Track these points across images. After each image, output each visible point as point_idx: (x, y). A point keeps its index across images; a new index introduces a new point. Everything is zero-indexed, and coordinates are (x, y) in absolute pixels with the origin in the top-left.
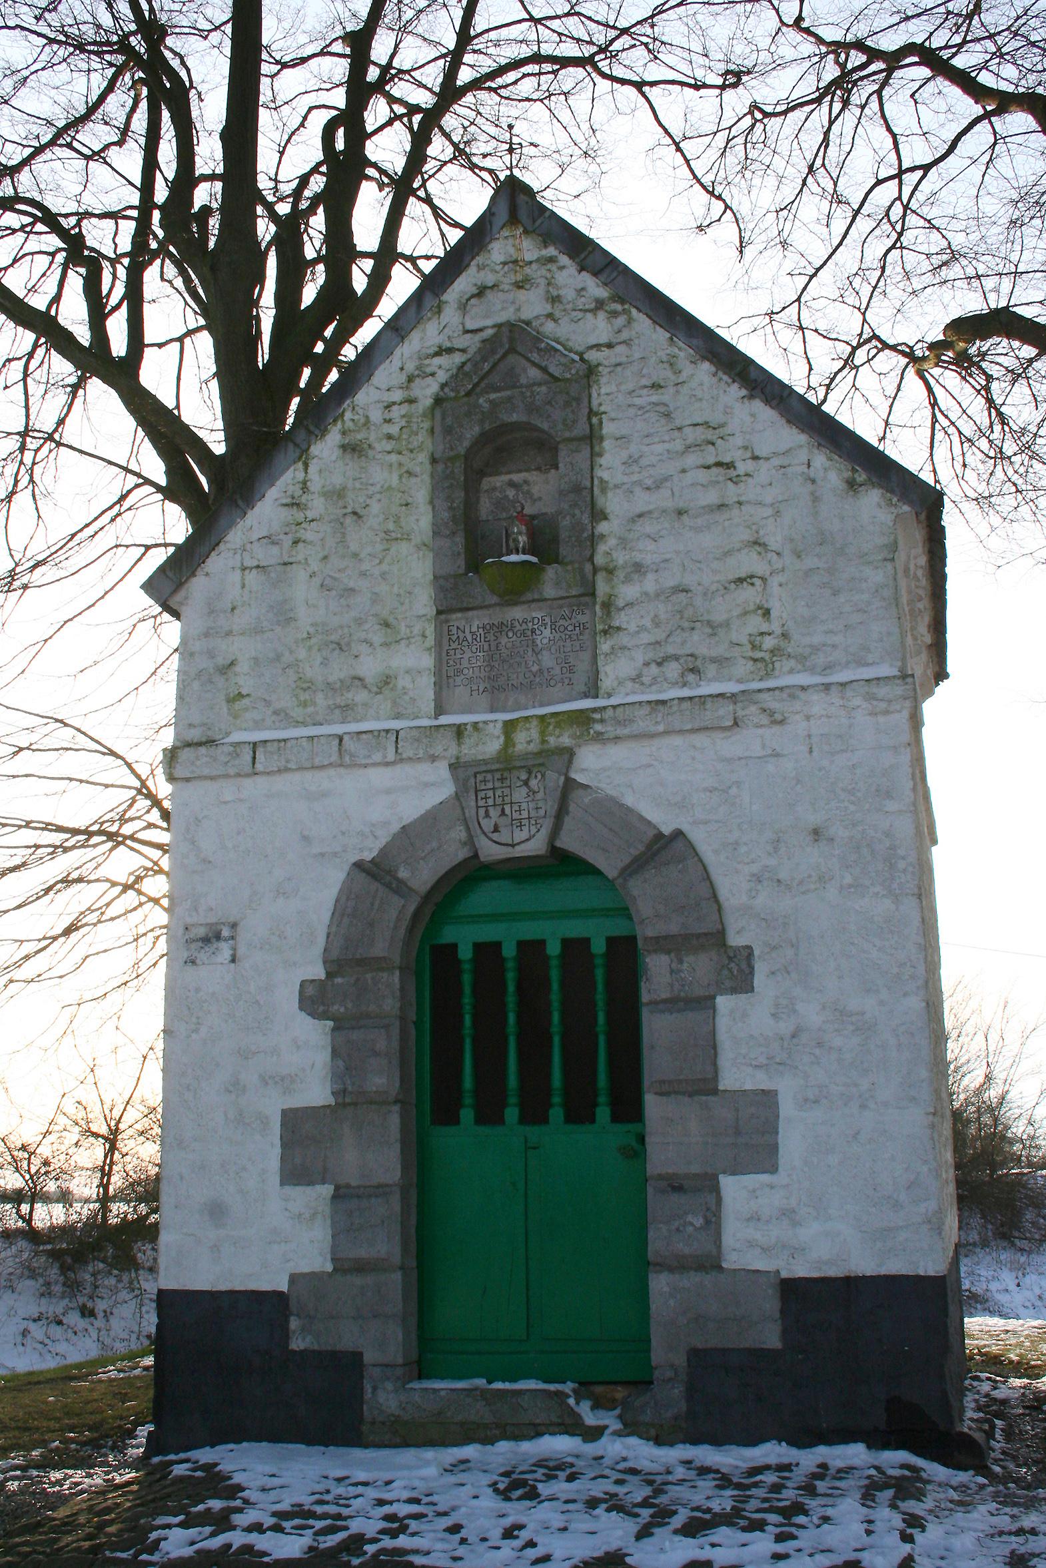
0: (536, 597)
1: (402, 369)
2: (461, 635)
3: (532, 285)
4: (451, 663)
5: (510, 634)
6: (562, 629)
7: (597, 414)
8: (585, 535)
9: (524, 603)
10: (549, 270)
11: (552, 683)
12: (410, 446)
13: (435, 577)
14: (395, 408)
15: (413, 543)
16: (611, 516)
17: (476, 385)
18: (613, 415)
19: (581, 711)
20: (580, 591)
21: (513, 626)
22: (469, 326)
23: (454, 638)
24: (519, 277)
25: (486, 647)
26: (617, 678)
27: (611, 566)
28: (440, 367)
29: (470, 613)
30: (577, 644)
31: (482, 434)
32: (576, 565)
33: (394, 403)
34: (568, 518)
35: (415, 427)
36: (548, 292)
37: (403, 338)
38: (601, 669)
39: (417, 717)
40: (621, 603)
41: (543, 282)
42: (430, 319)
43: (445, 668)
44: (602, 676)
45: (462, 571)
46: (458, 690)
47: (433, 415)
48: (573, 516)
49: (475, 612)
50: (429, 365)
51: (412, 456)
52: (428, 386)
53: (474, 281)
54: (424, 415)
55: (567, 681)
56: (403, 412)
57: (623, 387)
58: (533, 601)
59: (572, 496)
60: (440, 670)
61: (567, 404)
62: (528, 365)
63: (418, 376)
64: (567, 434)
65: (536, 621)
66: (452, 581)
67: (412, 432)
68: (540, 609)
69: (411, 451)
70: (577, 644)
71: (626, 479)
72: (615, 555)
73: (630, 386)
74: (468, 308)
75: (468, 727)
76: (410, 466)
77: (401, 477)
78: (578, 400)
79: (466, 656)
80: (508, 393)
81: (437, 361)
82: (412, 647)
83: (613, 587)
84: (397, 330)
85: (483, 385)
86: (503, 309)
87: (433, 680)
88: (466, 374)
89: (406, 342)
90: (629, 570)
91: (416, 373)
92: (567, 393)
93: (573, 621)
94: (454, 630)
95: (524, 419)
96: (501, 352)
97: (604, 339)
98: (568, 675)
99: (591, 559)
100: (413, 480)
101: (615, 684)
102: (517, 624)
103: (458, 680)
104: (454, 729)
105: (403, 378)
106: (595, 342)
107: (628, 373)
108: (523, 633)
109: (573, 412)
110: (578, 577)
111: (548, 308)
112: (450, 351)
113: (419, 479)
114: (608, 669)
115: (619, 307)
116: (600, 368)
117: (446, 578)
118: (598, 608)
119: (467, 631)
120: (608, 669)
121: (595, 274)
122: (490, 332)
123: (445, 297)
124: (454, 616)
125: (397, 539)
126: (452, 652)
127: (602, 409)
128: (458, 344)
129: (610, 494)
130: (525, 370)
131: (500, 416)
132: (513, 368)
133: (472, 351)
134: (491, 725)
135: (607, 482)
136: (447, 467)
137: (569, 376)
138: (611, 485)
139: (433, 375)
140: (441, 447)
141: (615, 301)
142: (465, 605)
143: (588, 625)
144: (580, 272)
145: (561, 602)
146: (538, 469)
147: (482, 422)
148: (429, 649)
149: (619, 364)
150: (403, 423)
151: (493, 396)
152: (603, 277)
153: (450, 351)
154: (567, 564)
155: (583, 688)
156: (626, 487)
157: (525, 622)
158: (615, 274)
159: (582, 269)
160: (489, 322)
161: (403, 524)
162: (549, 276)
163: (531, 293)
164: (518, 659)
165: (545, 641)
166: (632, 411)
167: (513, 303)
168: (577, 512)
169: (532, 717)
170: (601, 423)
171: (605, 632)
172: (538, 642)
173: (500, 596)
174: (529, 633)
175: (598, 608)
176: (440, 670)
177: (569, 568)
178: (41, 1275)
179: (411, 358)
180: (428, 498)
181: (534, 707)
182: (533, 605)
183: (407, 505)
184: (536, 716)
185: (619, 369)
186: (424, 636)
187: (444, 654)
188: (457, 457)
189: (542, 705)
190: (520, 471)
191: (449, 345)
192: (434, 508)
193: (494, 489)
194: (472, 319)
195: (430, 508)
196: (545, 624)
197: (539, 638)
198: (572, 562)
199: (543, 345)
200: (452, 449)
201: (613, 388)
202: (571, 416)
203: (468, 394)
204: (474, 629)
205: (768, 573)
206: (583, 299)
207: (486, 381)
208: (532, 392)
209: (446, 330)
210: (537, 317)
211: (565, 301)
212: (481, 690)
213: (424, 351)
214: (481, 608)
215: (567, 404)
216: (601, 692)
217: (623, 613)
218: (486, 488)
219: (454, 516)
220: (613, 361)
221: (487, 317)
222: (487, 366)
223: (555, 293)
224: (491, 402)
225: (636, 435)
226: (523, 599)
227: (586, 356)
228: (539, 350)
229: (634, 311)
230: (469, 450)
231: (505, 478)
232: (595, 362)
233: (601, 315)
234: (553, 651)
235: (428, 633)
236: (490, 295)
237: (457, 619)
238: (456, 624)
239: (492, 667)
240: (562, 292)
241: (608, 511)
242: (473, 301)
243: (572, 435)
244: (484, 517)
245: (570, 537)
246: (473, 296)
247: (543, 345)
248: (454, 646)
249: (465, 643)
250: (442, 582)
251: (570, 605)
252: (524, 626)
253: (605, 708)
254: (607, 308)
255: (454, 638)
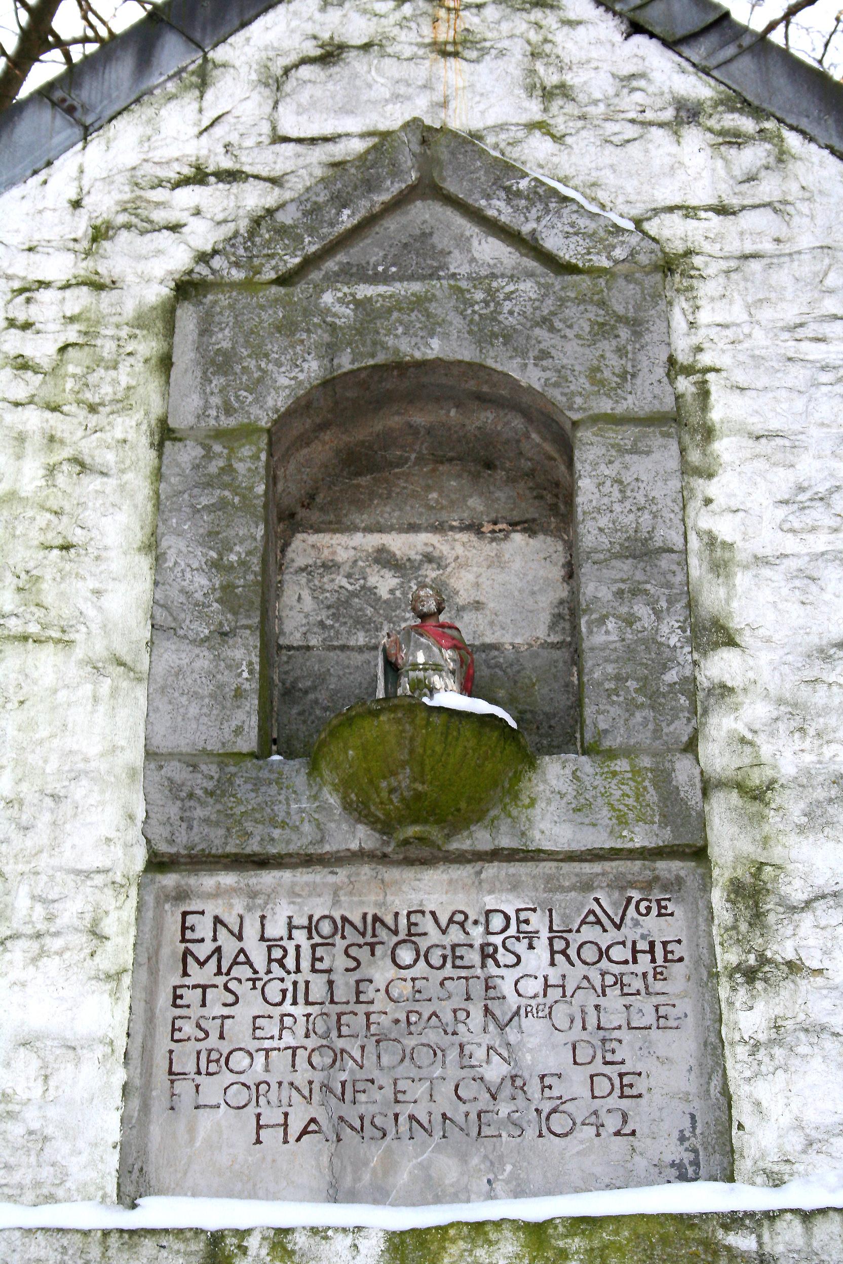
0: (506, 842)
1: (77, 204)
2: (230, 947)
3: (484, 52)
4: (188, 1029)
5: (406, 955)
6: (590, 954)
7: (688, 370)
8: (671, 676)
9: (461, 858)
10: (538, 26)
11: (559, 1123)
12: (88, 396)
13: (150, 755)
14: (44, 295)
15: (79, 652)
16: (745, 639)
17: (310, 262)
18: (740, 377)
19: (683, 1220)
20: (664, 837)
21: (413, 934)
22: (290, 125)
23: (202, 951)
24: (444, 34)
25: (318, 990)
26: (799, 1125)
27: (756, 778)
28: (197, 213)
29: (267, 878)
30: (646, 1005)
31: (328, 384)
32: (646, 762)
33: (43, 284)
34: (611, 624)
35: (107, 348)
36: (532, 72)
37: (86, 132)
38: (740, 1090)
39: (50, 1199)
40: (797, 892)
41: (518, 49)
42: (171, 98)
43: (163, 1043)
44: (742, 1112)
45: (249, 742)
46: (206, 1121)
47: (170, 329)
48: (630, 620)
49: (286, 876)
50: (158, 205)
51: (93, 420)
52: (159, 252)
53: (309, 28)
54: (140, 322)
55: (612, 1123)
56: (72, 309)
57: (766, 314)
58: (496, 855)
59: (626, 566)
60: (146, 1052)
61: (602, 330)
62: (470, 229)
63: (128, 226)
64: (605, 406)
65: (497, 922)
66: (214, 770)
67: (99, 361)
68: (515, 886)
69: (93, 409)
70: (646, 1005)
71: (790, 544)
72: (766, 750)
73: (790, 313)
74: (288, 87)
75: (253, 1243)
76: (88, 447)
77: (51, 471)
78: (637, 325)
79: (244, 1013)
80: (416, 287)
81: (188, 196)
82: (51, 965)
83: (765, 841)
84: (71, 110)
85: (331, 265)
86: (396, 97)
87: (120, 1076)
88: (282, 231)
89: (96, 144)
90: (820, 794)
91: (122, 219)
92: (602, 304)
93: (628, 932)
94: (204, 928)
95: (466, 353)
96: (391, 189)
97: (701, 196)
98: (613, 1101)
99: (691, 747)
100: (93, 483)
101: (795, 1142)
102: (427, 925)
103: (212, 1090)
104: (198, 1246)
105: (81, 226)
106: (677, 200)
107: (782, 277)
108: (454, 955)
109: (621, 351)
110: (652, 796)
111: (534, 110)
112: (230, 176)
113: (112, 482)
114: (762, 1090)
115: (747, 124)
116: (697, 261)
117: (192, 762)
118: (717, 897)
119: (251, 931)
120: (762, 1090)
121: (672, 44)
122: (358, 146)
123: (220, 54)
124: (208, 881)
125: (25, 638)
126: (192, 997)
127: (706, 359)
128: (251, 162)
129: (742, 579)
130: (463, 242)
131: (390, 341)
132: (425, 236)
133: (296, 186)
134: (342, 1243)
135: (728, 546)
136: (209, 456)
137: (606, 263)
138: (742, 556)
139: (175, 228)
140: (195, 401)
141: (732, 110)
142: (253, 846)
143: (678, 951)
144: (628, 36)
145: (587, 868)
146: (474, 528)
147: (330, 350)
148: (114, 977)
149: (754, 256)
150: (72, 334)
151: (365, 291)
152: (697, 52)
153: (230, 176)
154: (611, 754)
155: (675, 1152)
156: (792, 564)
157: (459, 920)
158: (730, 51)
159: (636, 28)
160: (353, 125)
161: (49, 599)
162: (534, 36)
163: (482, 67)
164: (433, 1036)
165: (532, 987)
166: (797, 375)
167: (427, 86)
168: (642, 610)
169: (498, 1224)
170: (704, 394)
171: (750, 975)
172: (506, 988)
173: (385, 827)
174: (474, 957)
175: (717, 897)
176: (146, 1052)
177: (622, 765)
178: (394, 623)
179: (108, 180)
180: (139, 536)
181: (491, 1196)
182: (492, 870)
183: (66, 547)
184: (518, 1226)
185: (755, 266)
186: (96, 934)
187: (164, 998)
188: (247, 432)
189: (519, 1192)
190: (413, 528)
191: (227, 164)
192: (159, 560)
193: (329, 566)
194: (301, 110)
195: (144, 563)
196: (531, 939)
197: (511, 975)
198: (628, 752)
199: (523, 184)
200: (228, 410)
201: (737, 313)
202: (614, 361)
203: (285, 280)
204: (276, 929)
205: (636, 1144)
206: (638, 97)
207: (342, 257)
208: (491, 293)
209: (218, 131)
210: (502, 127)
211: (582, 98)
212: (295, 1128)
213: (149, 169)
214: (308, 861)
215: (602, 330)
216: (744, 1166)
217: (807, 920)
218: (301, 562)
219: (227, 588)
220: (734, 246)
221: (346, 110)
222: (347, 219)
223: (552, 78)
224: (359, 304)
225: (814, 431)
226: (460, 844)
227: (646, 226)
228: (512, 195)
229: (793, 140)
230: (284, 419)
231: (373, 541)
232: (679, 247)
233: (693, 137)
234: (560, 1017)
235: (109, 926)
236: (357, 63)
237: (217, 893)
238: (212, 908)
239: (339, 1055)
240: (569, 78)
241: (736, 623)
242: (305, 71)
243: (620, 409)
244: (296, 639)
245: (619, 679)
246: (305, 61)
247: (523, 184)
248: (198, 975)
249: (243, 972)
250: (176, 771)
251: (620, 884)
252: (455, 935)
253: (771, 1216)
254: (712, 123)
255: (202, 951)
